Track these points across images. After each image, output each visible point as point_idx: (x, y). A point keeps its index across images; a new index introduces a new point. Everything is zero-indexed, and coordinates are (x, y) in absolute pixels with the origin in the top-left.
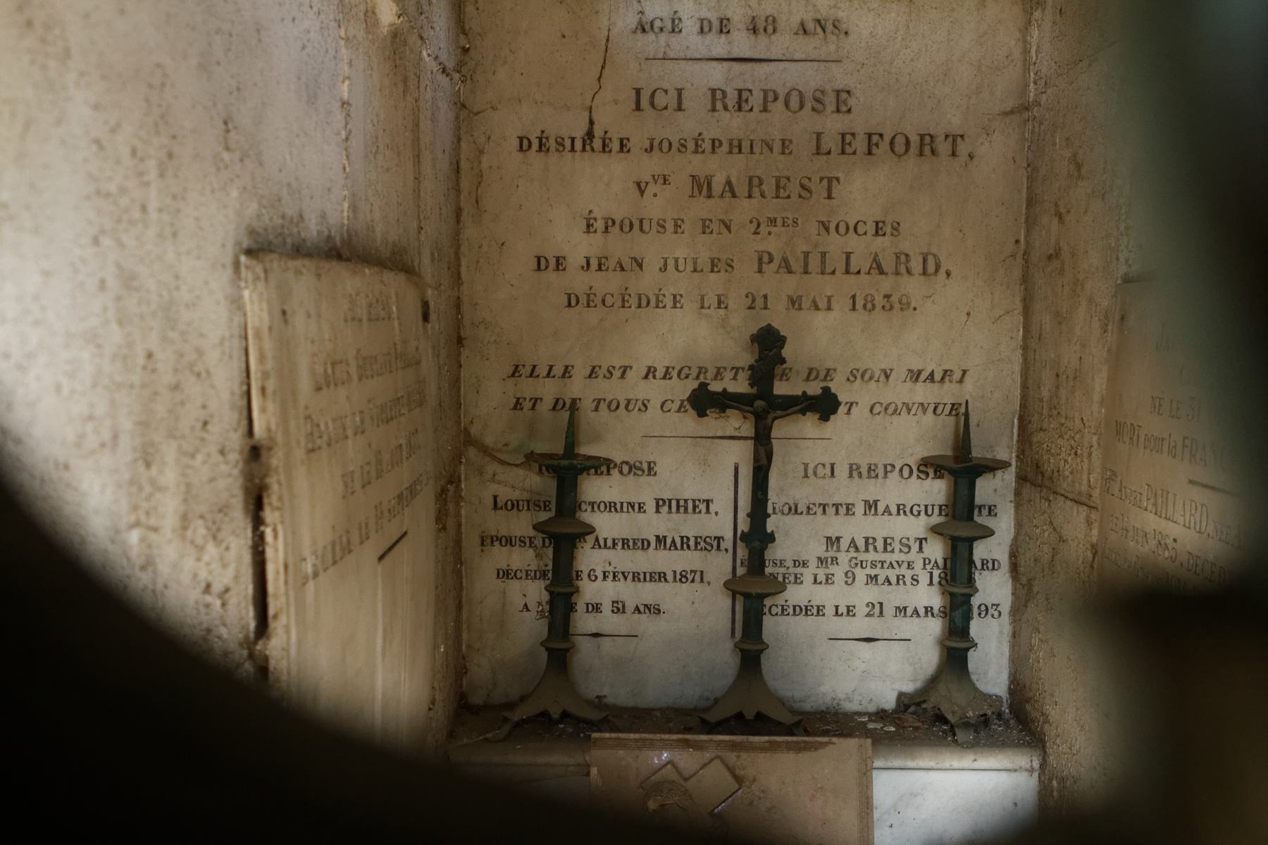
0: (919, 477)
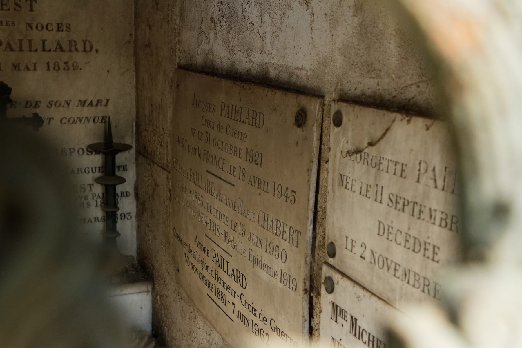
0: (88, 154)
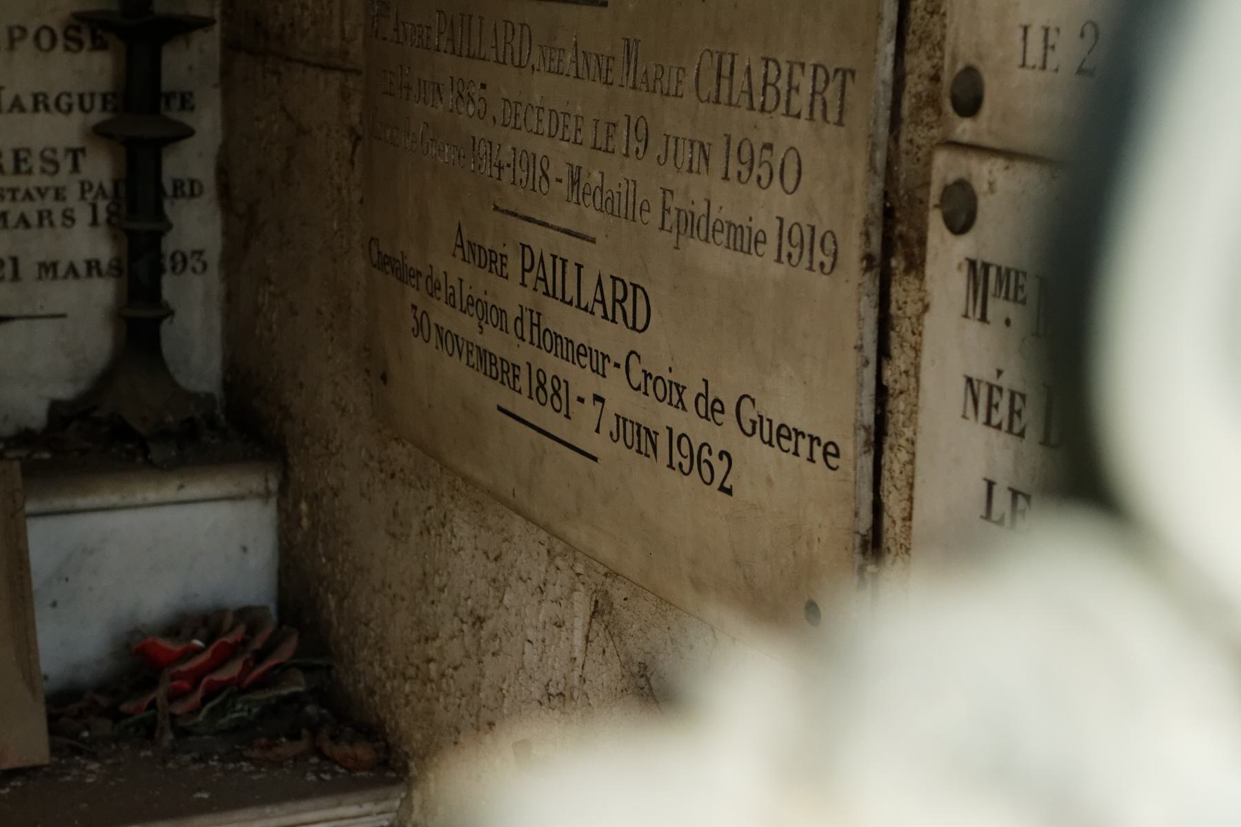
0: (67, 48)
